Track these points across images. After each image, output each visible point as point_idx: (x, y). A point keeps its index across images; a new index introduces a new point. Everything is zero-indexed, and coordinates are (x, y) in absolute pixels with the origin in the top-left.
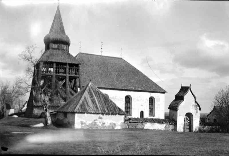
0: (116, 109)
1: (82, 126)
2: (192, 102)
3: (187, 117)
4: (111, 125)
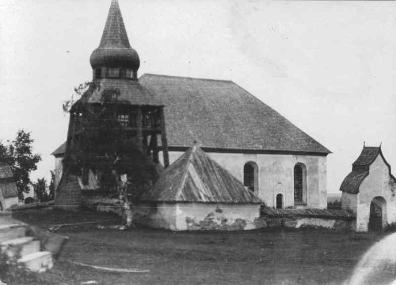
0: (245, 193)
1: (188, 226)
2: (384, 176)
4: (237, 223)
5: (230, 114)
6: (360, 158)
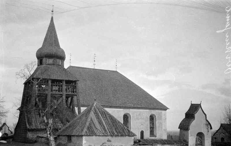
3: (198, 137)
5: (115, 88)
6: (189, 110)
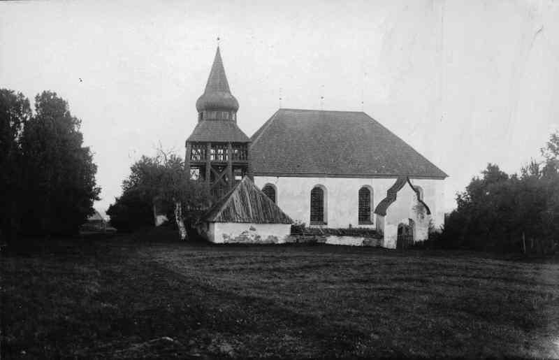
5: (352, 142)
